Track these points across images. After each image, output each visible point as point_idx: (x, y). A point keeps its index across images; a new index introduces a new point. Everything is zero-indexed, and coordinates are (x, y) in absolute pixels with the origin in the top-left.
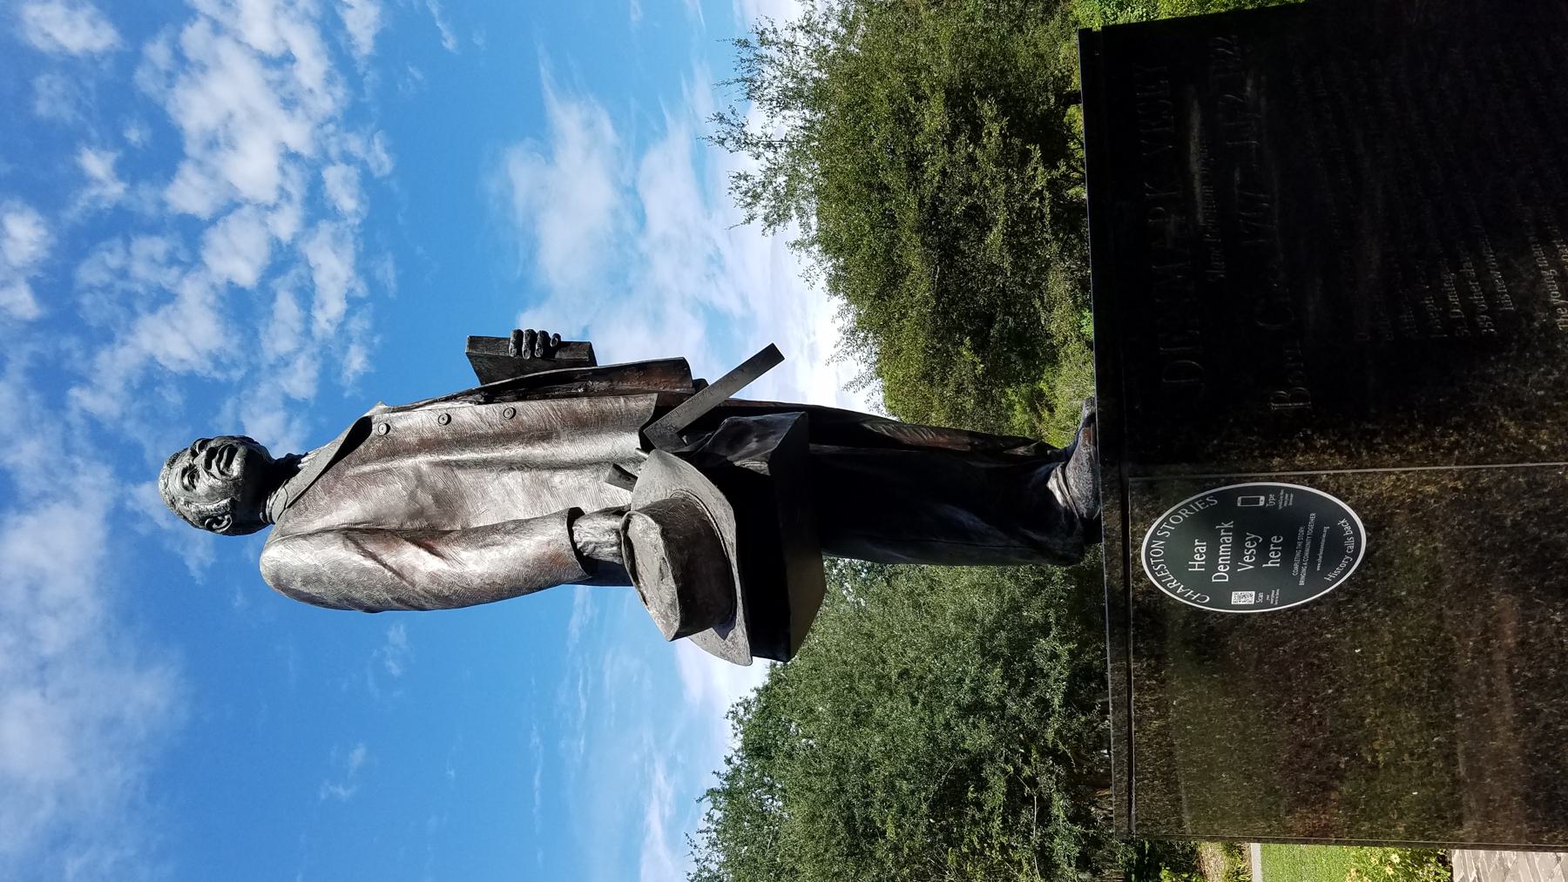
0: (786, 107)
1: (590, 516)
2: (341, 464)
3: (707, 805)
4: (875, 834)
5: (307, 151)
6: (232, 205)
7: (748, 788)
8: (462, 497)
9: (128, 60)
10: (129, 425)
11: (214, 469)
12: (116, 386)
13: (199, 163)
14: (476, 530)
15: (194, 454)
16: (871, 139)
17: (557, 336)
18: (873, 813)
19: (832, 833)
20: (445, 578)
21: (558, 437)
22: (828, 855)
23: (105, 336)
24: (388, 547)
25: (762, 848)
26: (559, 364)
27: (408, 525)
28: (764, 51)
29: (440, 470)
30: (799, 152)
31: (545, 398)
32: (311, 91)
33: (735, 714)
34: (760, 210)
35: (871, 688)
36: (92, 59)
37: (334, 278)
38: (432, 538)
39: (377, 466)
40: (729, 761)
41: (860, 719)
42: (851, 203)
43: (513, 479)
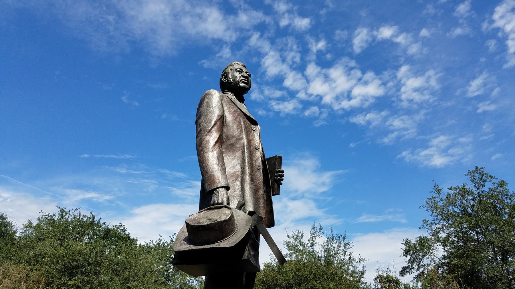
0: (325, 251)
1: (227, 194)
2: (243, 116)
3: (89, 215)
4: (71, 276)
5: (323, 102)
6: (308, 81)
7: (93, 230)
8: (233, 152)
9: (351, 56)
10: (247, 48)
11: (242, 78)
12: (259, 44)
13: (320, 73)
14: (223, 156)
15: (246, 73)
16: (316, 281)
17: (282, 184)
18: (79, 276)
19: (74, 261)
20: (208, 146)
21: (252, 184)
22: (65, 259)
23: (273, 42)
24: (218, 129)
25: (71, 234)
26: (273, 184)
27: (224, 135)
28: (342, 244)
29: (242, 146)
30: (311, 254)
31: (263, 180)
32: (340, 104)
33: (121, 226)
34: (292, 240)
35: (125, 276)
36: (351, 46)
37: (286, 108)
38: (221, 142)
39: (243, 126)
40: (104, 223)
41: (115, 272)
42: (295, 272)
43: (238, 168)
